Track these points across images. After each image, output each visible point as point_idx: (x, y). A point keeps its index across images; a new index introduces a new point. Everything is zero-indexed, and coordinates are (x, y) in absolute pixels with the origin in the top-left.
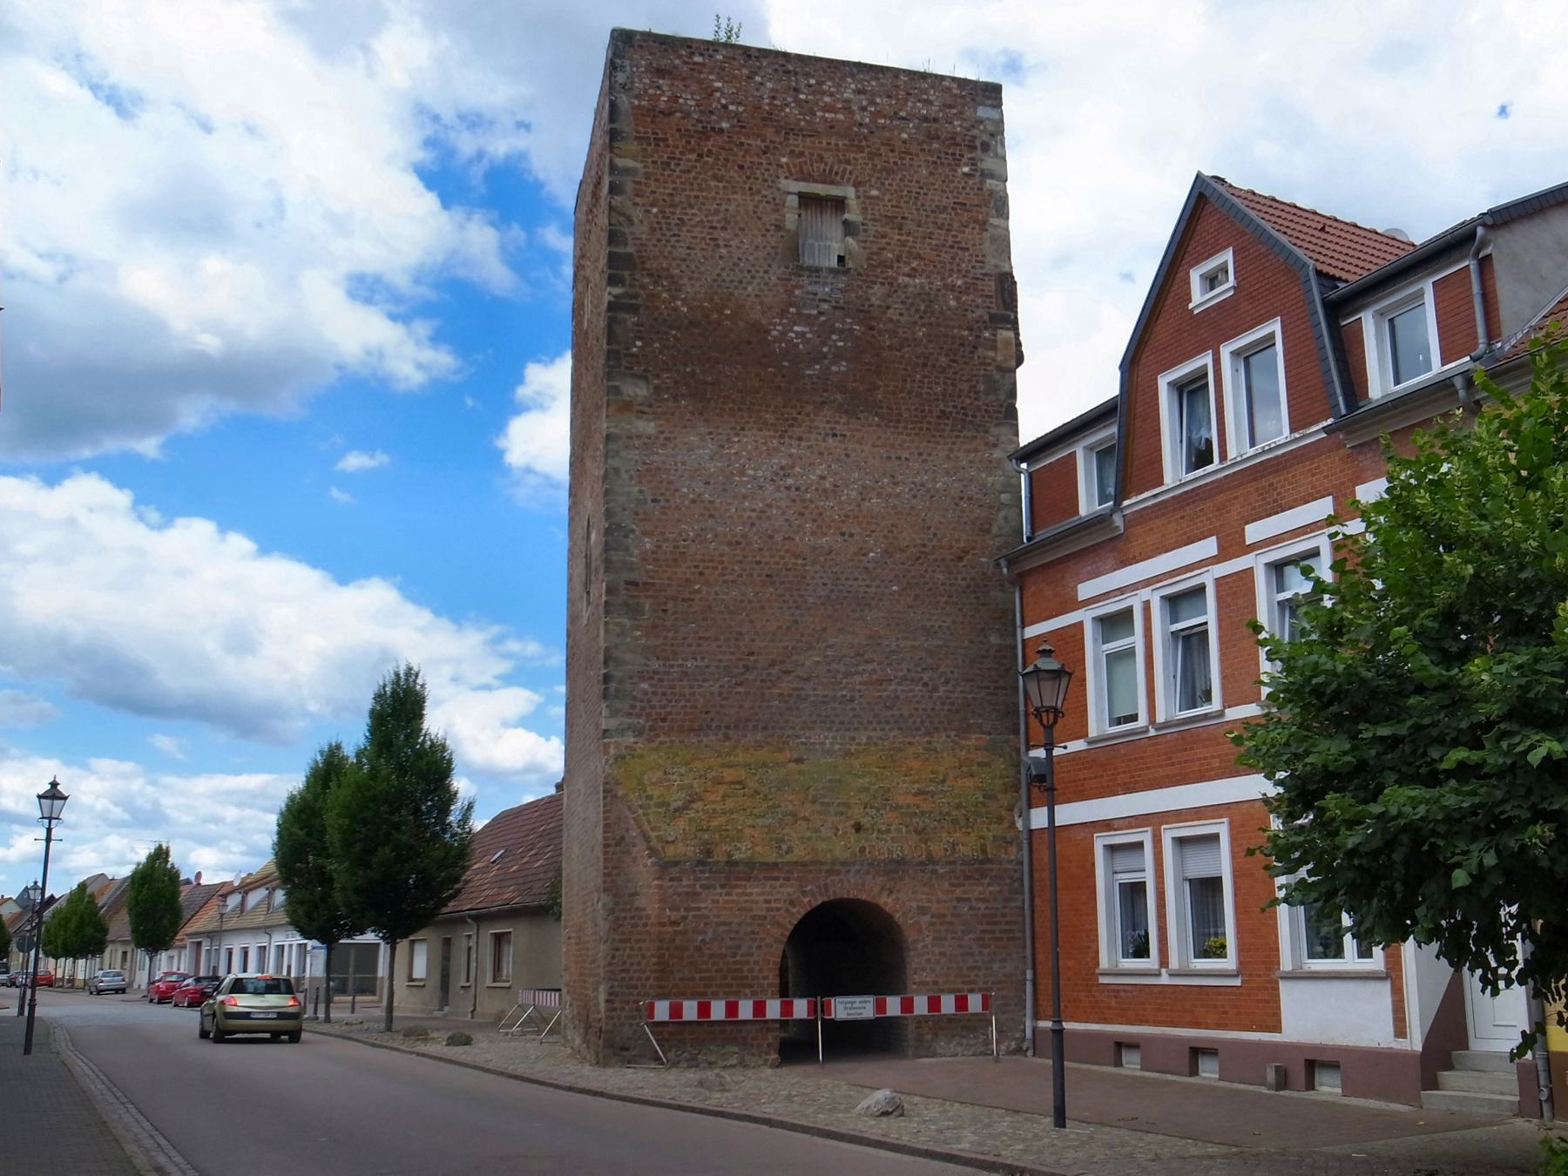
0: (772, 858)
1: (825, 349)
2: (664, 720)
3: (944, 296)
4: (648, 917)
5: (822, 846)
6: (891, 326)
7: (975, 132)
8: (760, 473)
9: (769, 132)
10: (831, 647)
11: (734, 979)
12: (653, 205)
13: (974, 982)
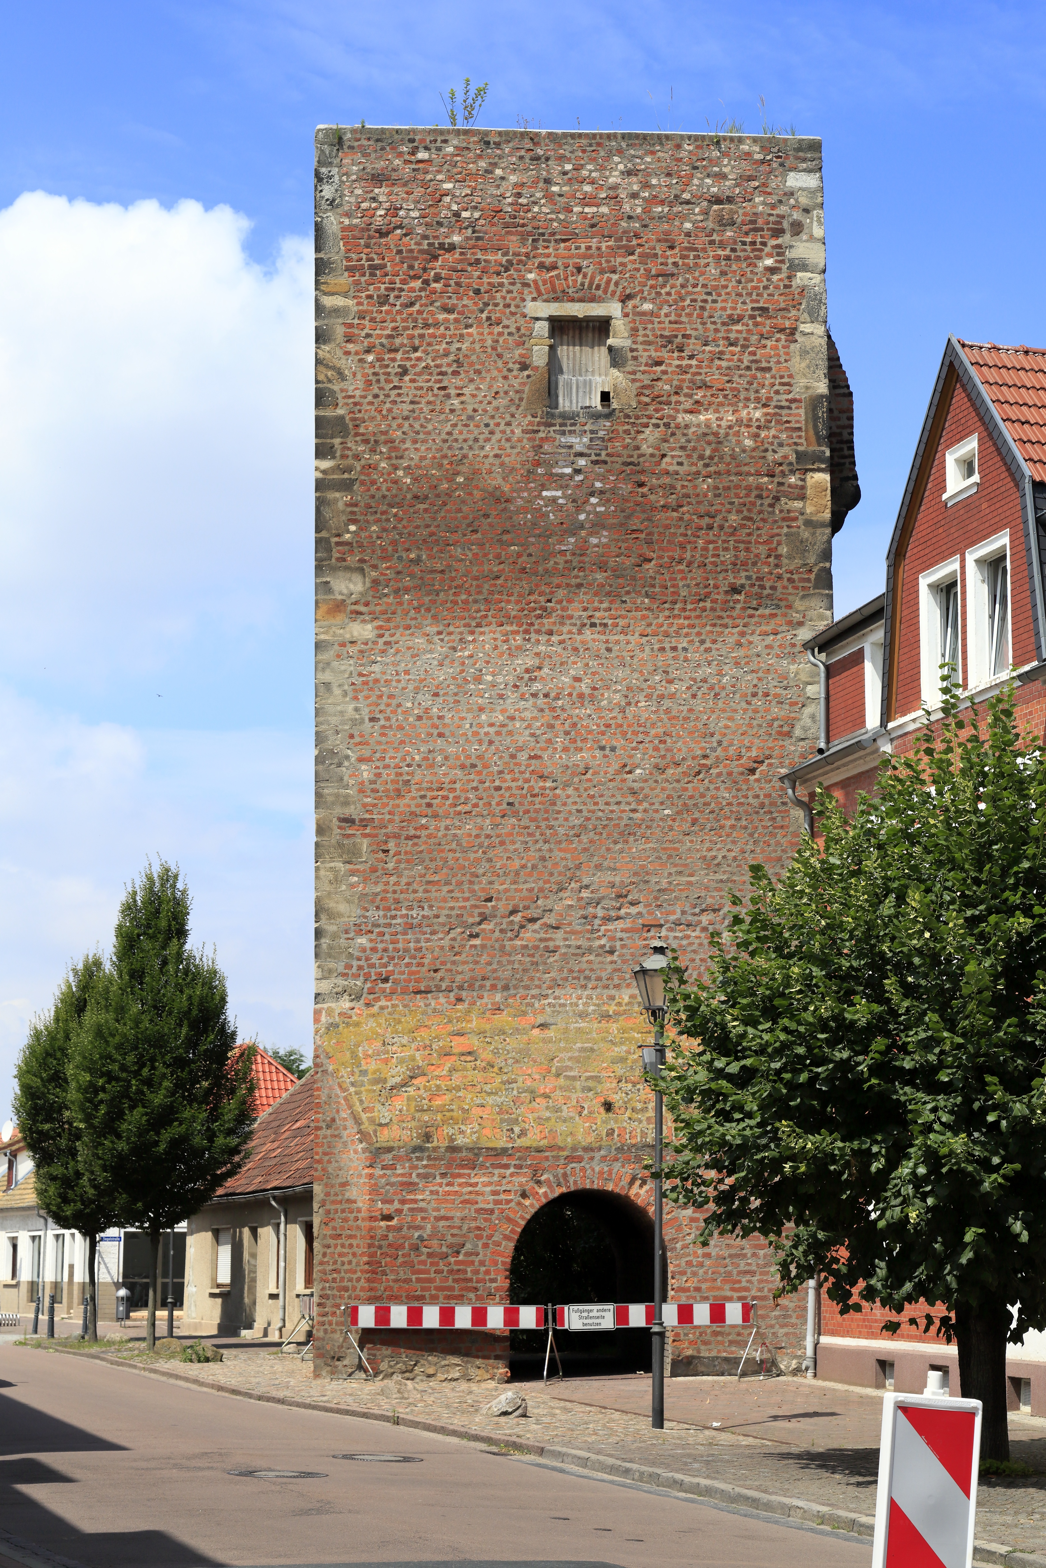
0: (502, 1143)
1: (582, 517)
2: (386, 980)
3: (737, 434)
4: (359, 1211)
5: (562, 1128)
6: (667, 480)
7: (782, 210)
8: (500, 679)
9: (513, 242)
10: (587, 887)
11: (455, 1280)
12: (368, 351)
13: (747, 1289)
